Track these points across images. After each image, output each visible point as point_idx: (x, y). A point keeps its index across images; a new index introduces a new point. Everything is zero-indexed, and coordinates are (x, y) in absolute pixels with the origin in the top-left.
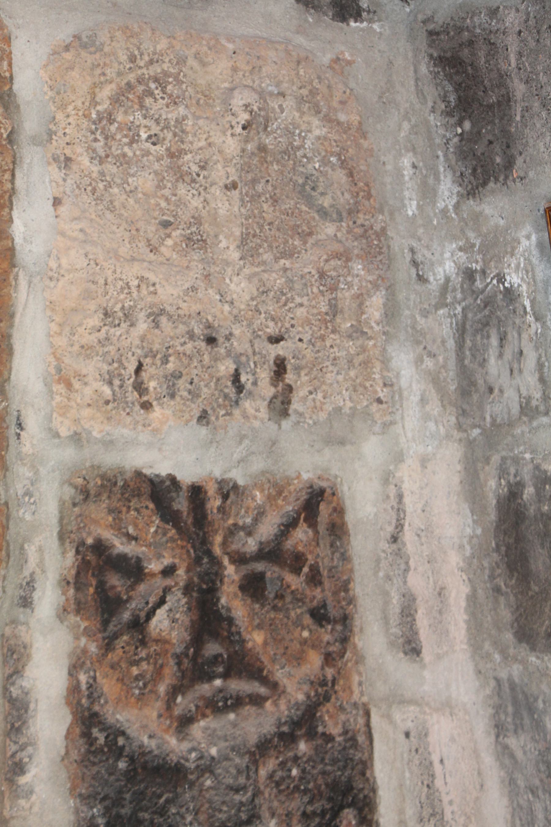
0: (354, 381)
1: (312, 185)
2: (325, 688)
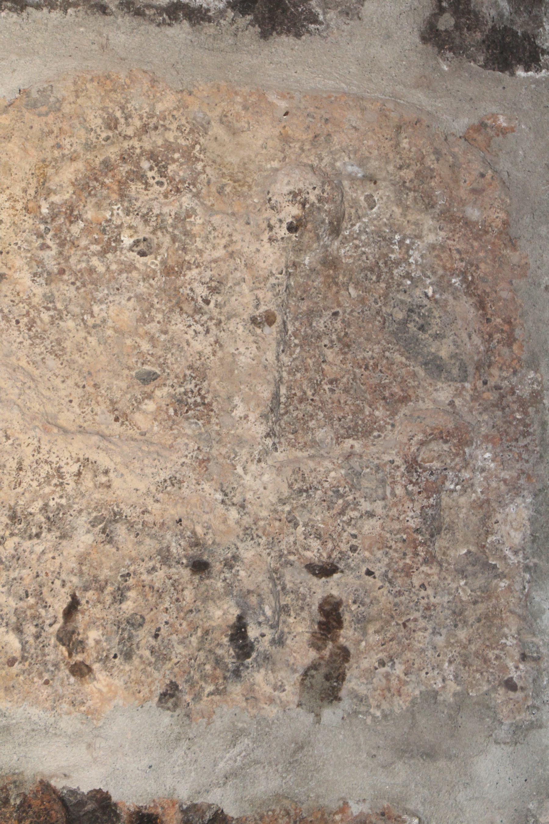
0: (465, 647)
1: (421, 322)
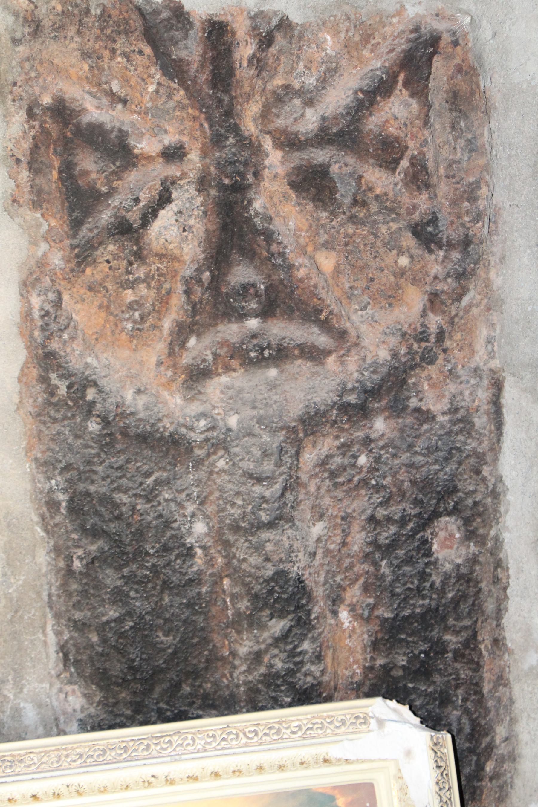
2: (424, 345)
